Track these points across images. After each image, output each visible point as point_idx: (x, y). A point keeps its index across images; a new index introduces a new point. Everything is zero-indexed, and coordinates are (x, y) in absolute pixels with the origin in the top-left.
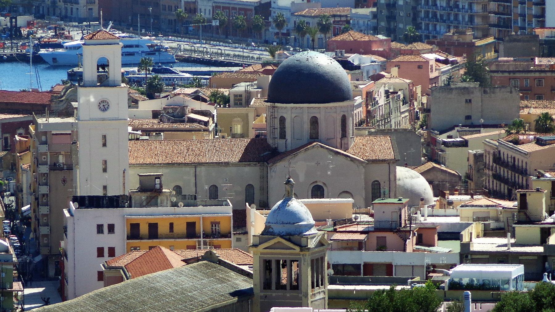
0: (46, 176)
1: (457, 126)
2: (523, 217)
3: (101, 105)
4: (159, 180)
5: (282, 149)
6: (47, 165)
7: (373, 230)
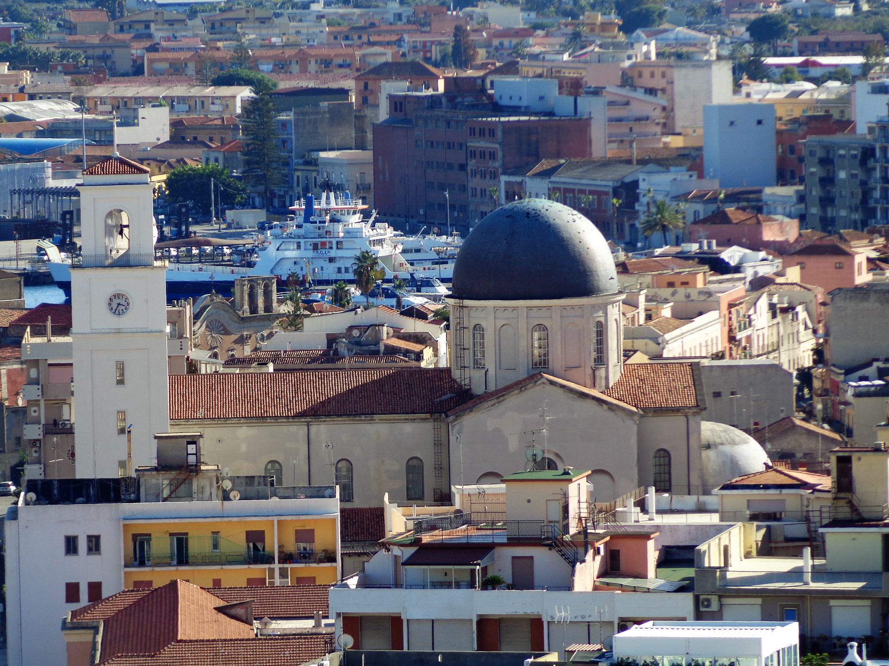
0: (38, 445)
1: (877, 360)
2: (844, 512)
3: (116, 301)
4: (194, 446)
5: (478, 389)
6: (39, 423)
7: (505, 541)
